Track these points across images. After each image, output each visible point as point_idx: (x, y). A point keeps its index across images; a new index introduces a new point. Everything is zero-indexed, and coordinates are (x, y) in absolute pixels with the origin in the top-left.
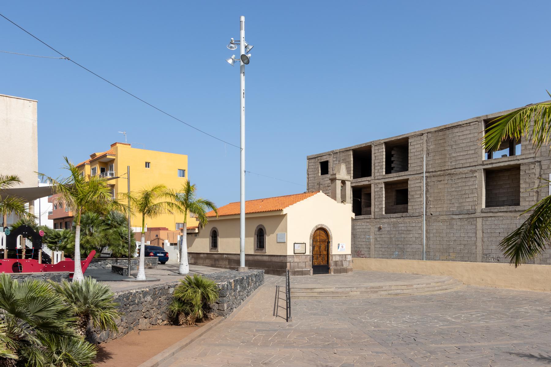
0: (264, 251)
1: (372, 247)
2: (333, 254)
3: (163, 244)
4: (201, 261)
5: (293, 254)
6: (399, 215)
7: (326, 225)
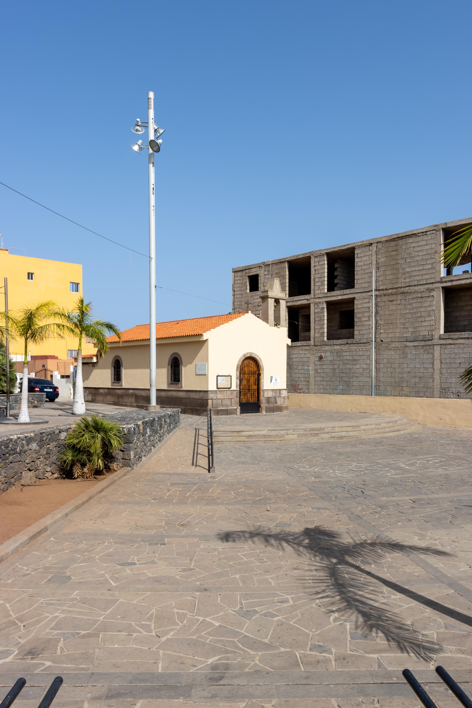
0: (179, 385)
1: (312, 380)
2: (265, 388)
3: (52, 376)
4: (100, 398)
5: (216, 389)
6: (344, 341)
7: (252, 352)
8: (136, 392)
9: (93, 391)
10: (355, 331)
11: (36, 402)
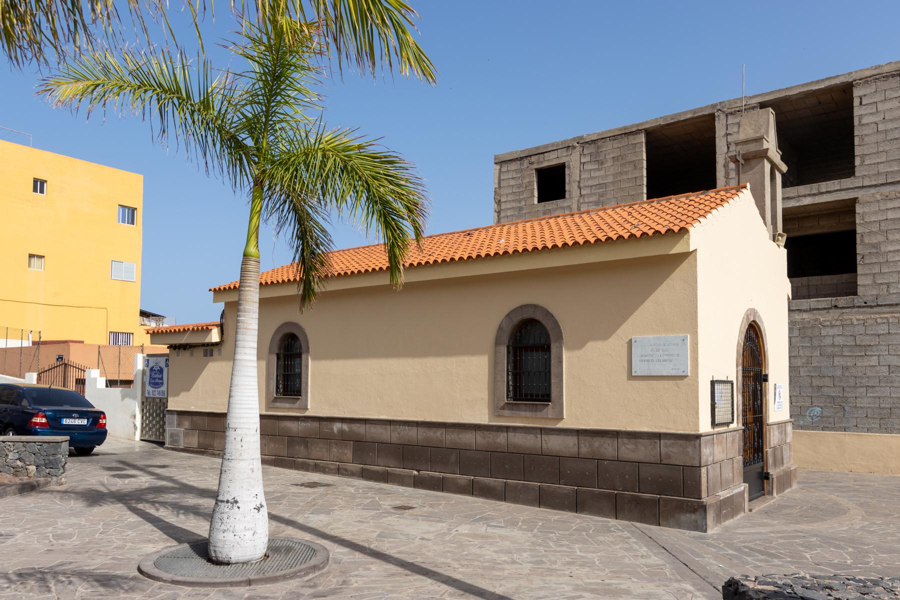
0: (550, 410)
3: (81, 382)
6: (824, 302)
8: (360, 429)
10: (859, 278)
11: (33, 468)
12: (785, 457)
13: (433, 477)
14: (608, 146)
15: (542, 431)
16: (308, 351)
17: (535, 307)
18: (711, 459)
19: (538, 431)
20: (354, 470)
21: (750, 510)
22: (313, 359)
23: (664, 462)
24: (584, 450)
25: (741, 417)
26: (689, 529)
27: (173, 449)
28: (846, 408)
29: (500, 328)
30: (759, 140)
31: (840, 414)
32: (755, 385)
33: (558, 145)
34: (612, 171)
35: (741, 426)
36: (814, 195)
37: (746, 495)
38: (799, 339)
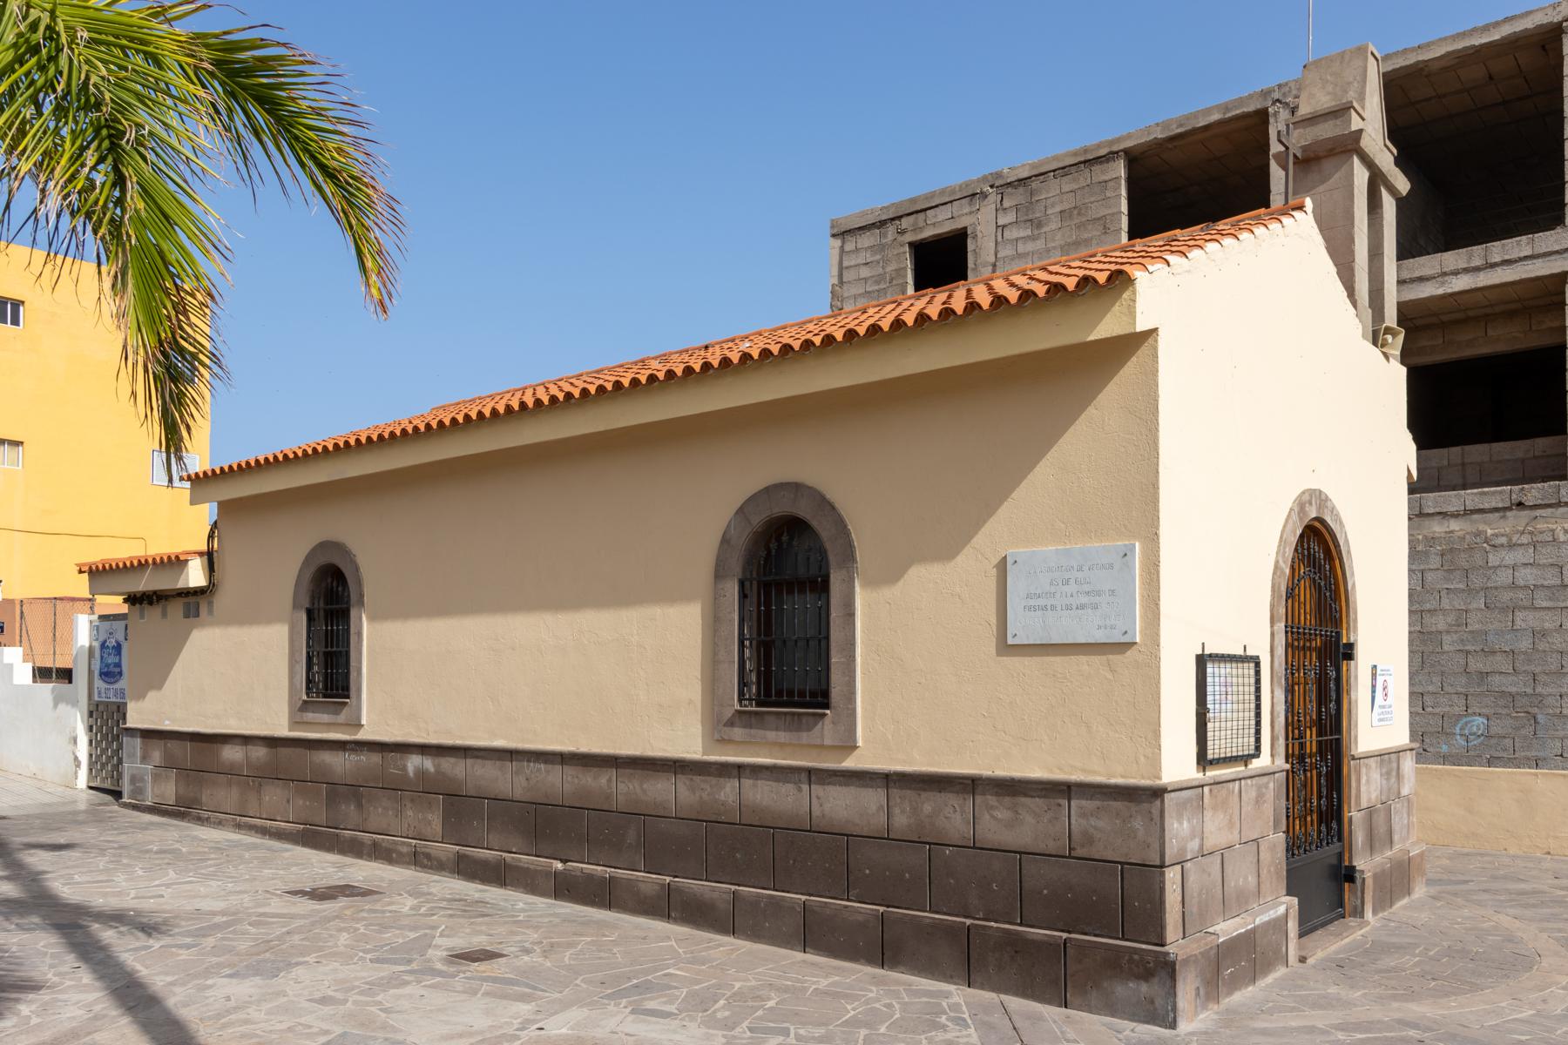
0: (827, 730)
4: (223, 795)
6: (1496, 495)
8: (455, 768)
9: (185, 750)
12: (1396, 827)
13: (590, 877)
14: (1052, 188)
15: (812, 775)
16: (361, 603)
17: (796, 488)
18: (1194, 845)
19: (804, 776)
20: (443, 856)
21: (1303, 960)
22: (371, 619)
23: (1079, 852)
24: (901, 821)
25: (1282, 741)
26: (1133, 1017)
27: (135, 807)
28: (1540, 718)
29: (725, 541)
30: (1341, 111)
31: (1528, 731)
32: (1323, 667)
33: (953, 192)
34: (1059, 240)
35: (1281, 763)
36: (1477, 269)
37: (1293, 927)
38: (1440, 574)
